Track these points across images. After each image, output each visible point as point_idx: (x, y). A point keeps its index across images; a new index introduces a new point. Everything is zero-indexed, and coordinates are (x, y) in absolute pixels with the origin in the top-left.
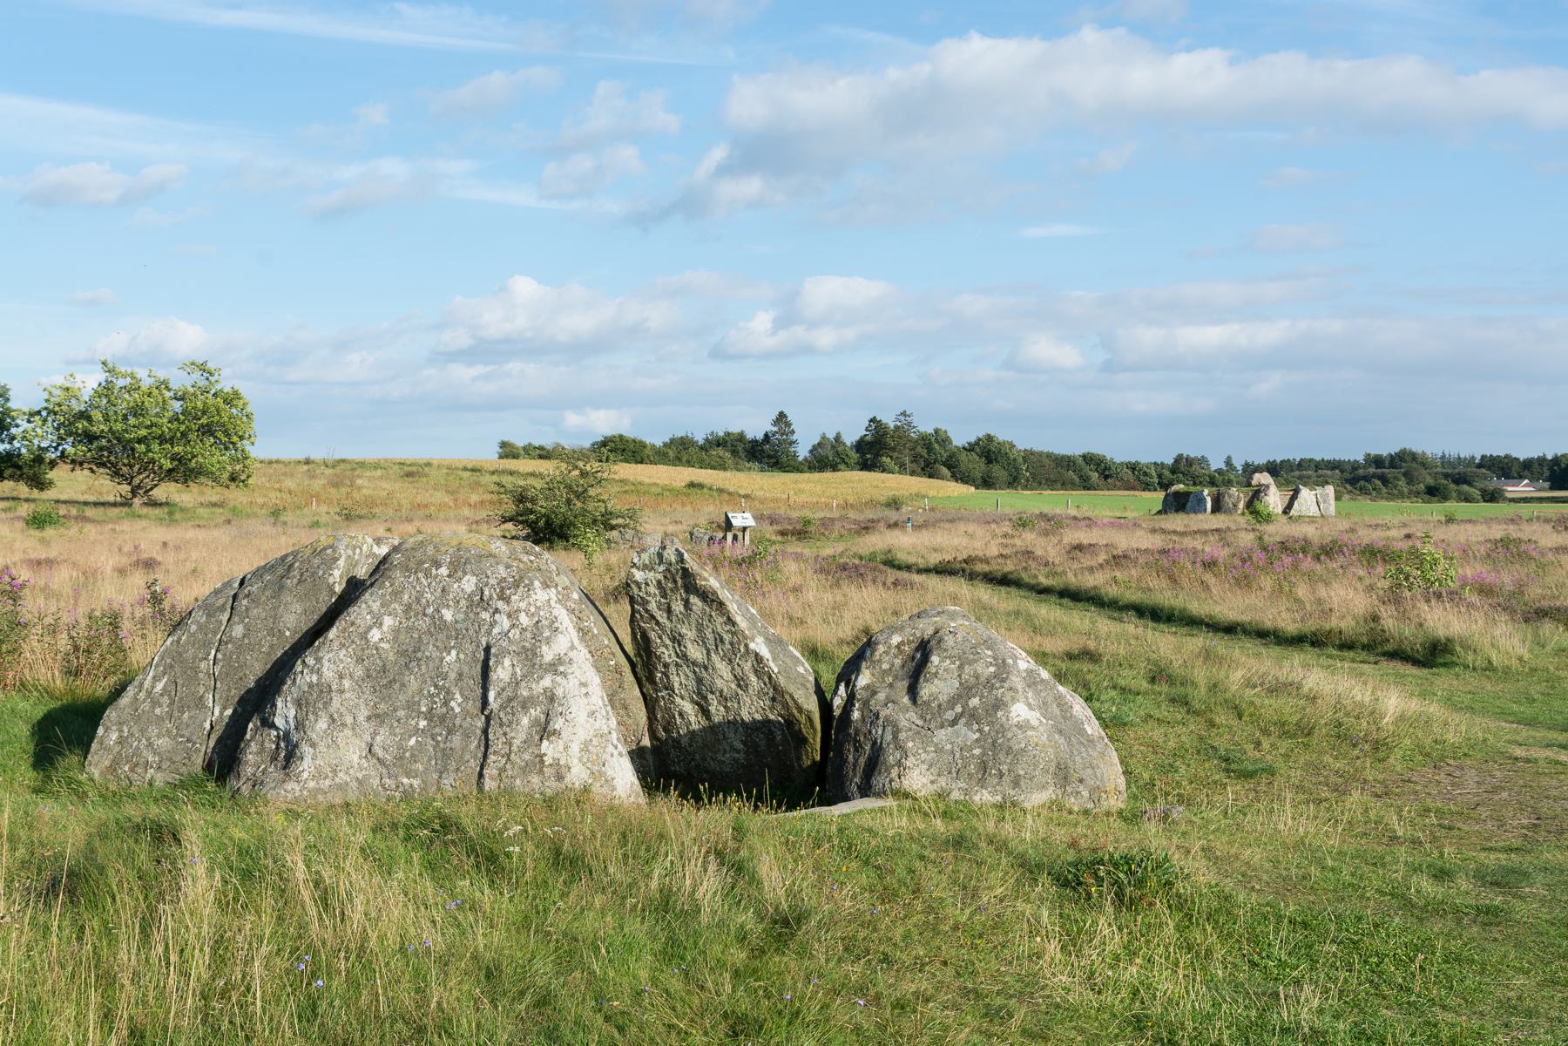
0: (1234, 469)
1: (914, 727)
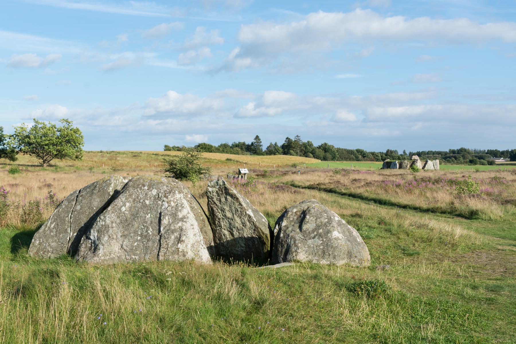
0: (406, 154)
1: (301, 239)
